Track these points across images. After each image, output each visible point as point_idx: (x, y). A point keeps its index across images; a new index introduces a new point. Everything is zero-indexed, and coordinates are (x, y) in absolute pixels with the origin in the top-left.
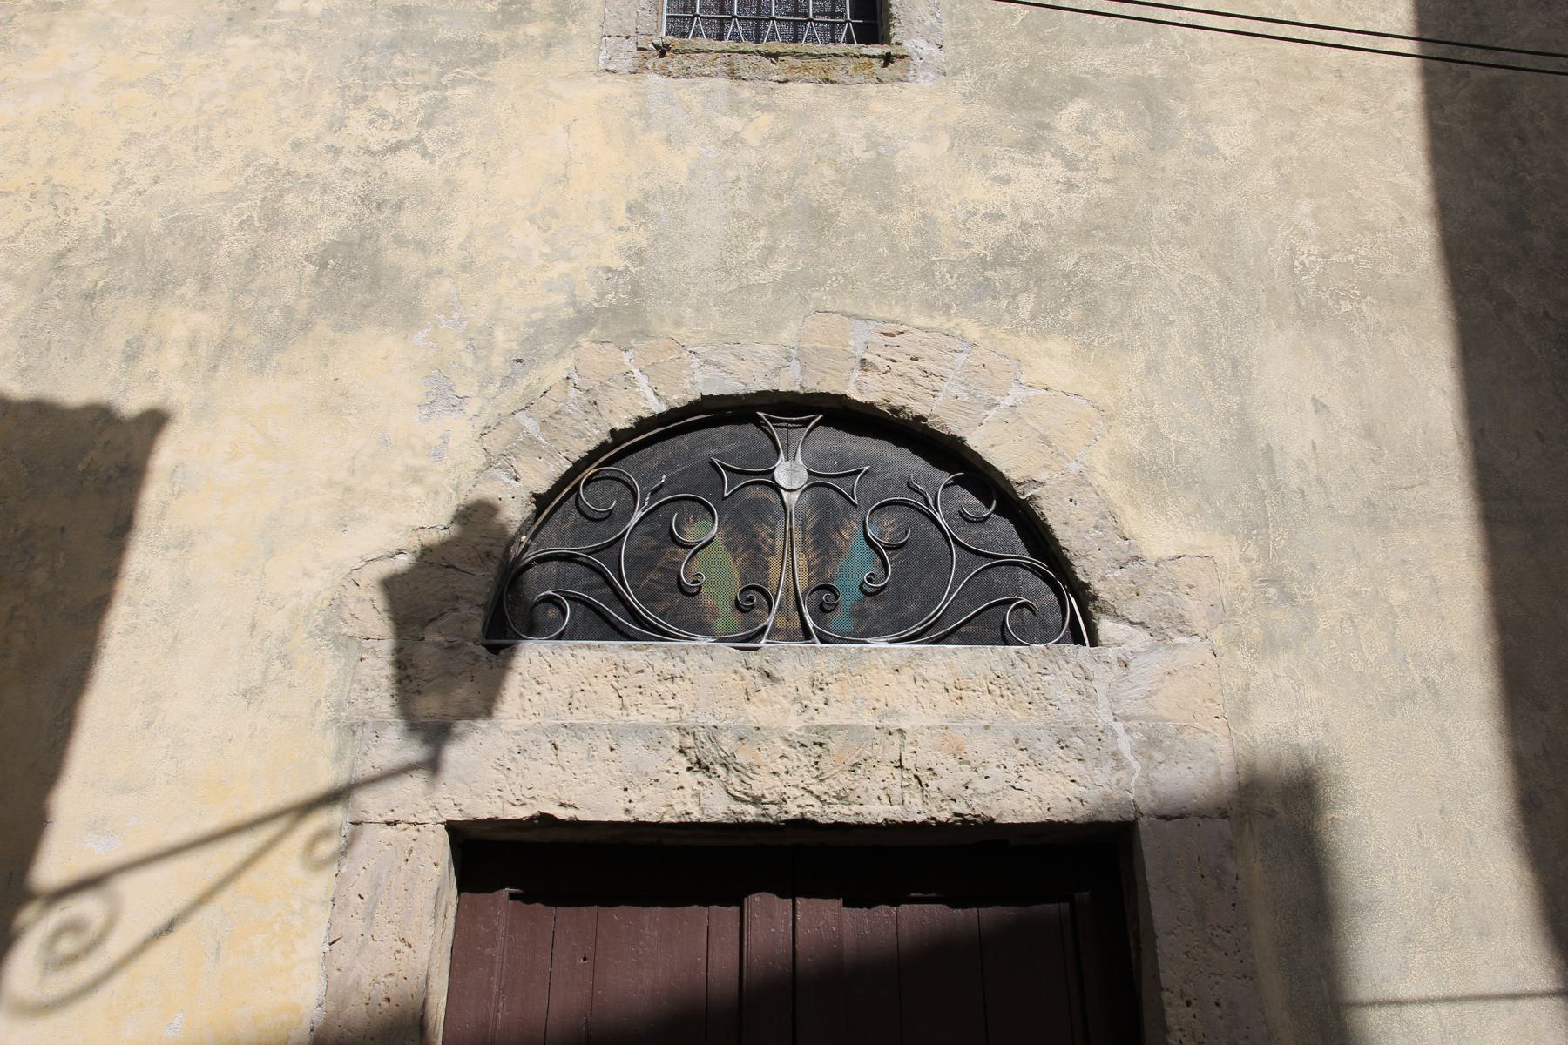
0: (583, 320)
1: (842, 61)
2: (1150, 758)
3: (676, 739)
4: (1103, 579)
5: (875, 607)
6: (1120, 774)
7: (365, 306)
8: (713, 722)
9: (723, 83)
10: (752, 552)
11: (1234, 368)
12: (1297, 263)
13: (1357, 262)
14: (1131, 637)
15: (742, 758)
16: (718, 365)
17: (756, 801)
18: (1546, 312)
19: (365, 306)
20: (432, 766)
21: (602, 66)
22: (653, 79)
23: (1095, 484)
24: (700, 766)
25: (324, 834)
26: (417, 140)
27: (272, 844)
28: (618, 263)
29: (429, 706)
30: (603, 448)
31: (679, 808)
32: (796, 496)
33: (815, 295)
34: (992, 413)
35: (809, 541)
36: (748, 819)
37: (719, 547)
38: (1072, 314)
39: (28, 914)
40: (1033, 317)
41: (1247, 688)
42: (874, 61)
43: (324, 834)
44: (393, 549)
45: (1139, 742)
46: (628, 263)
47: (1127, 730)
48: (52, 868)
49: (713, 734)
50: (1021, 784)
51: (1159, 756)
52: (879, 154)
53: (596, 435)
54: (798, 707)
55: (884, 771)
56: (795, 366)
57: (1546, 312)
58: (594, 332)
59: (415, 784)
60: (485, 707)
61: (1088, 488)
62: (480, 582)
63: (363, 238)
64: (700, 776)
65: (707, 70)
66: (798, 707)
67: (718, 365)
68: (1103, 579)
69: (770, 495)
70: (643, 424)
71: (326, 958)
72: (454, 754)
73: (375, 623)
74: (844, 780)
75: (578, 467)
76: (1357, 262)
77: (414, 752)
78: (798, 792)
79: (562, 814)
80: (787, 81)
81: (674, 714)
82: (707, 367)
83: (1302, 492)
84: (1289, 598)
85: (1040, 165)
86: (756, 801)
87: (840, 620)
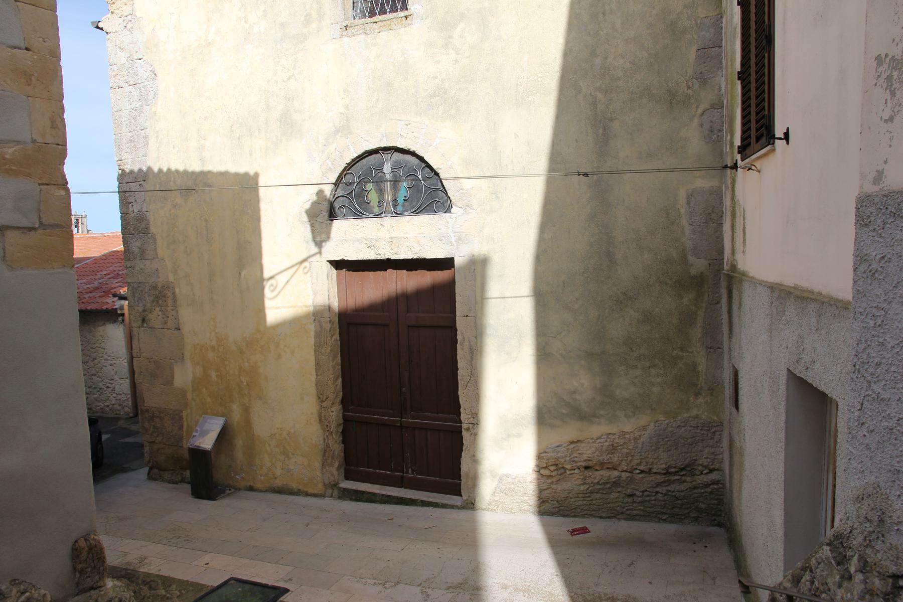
0: (337, 131)
1: (394, 20)
2: (459, 242)
3: (364, 241)
4: (453, 196)
5: (407, 204)
6: (452, 247)
7: (291, 133)
8: (599, 67)
9: (363, 36)
10: (381, 192)
11: (494, 125)
12: (519, 83)
13: (537, 79)
14: (459, 211)
15: (376, 245)
16: (368, 141)
17: (380, 255)
18: (591, 93)
19: (291, 133)
20: (320, 253)
21: (332, 38)
22: (346, 39)
23: (453, 167)
24: (369, 247)
25: (305, 267)
26: (293, 75)
27: (297, 269)
28: (343, 111)
29: (318, 239)
30: (346, 167)
31: (366, 257)
32: (388, 175)
33: (389, 115)
34: (431, 148)
35: (392, 187)
36: (379, 258)
37: (373, 190)
38: (453, 111)
39: (265, 283)
40: (442, 114)
41: (484, 223)
42: (403, 18)
43: (305, 267)
44: (308, 199)
45: (457, 239)
46: (345, 110)
47: (454, 236)
48: (266, 275)
49: (371, 239)
50: (431, 250)
51: (461, 242)
52: (405, 58)
53: (344, 165)
54: (388, 232)
55: (404, 247)
56: (385, 139)
57: (591, 93)
58: (340, 134)
59: (318, 256)
60: (328, 238)
61: (452, 169)
62: (325, 207)
63: (288, 111)
64: (370, 249)
65: (358, 33)
66: (388, 232)
67: (368, 141)
68: (453, 196)
69: (383, 175)
70: (353, 160)
71: (312, 287)
72: (323, 250)
73: (305, 218)
74: (396, 250)
75: (341, 174)
76: (537, 79)
77: (316, 250)
78: (387, 252)
79: (346, 259)
80: (380, 32)
81: (364, 235)
82: (365, 142)
83: (507, 165)
84: (497, 198)
85: (448, 54)
86: (380, 255)
87: (399, 208)
